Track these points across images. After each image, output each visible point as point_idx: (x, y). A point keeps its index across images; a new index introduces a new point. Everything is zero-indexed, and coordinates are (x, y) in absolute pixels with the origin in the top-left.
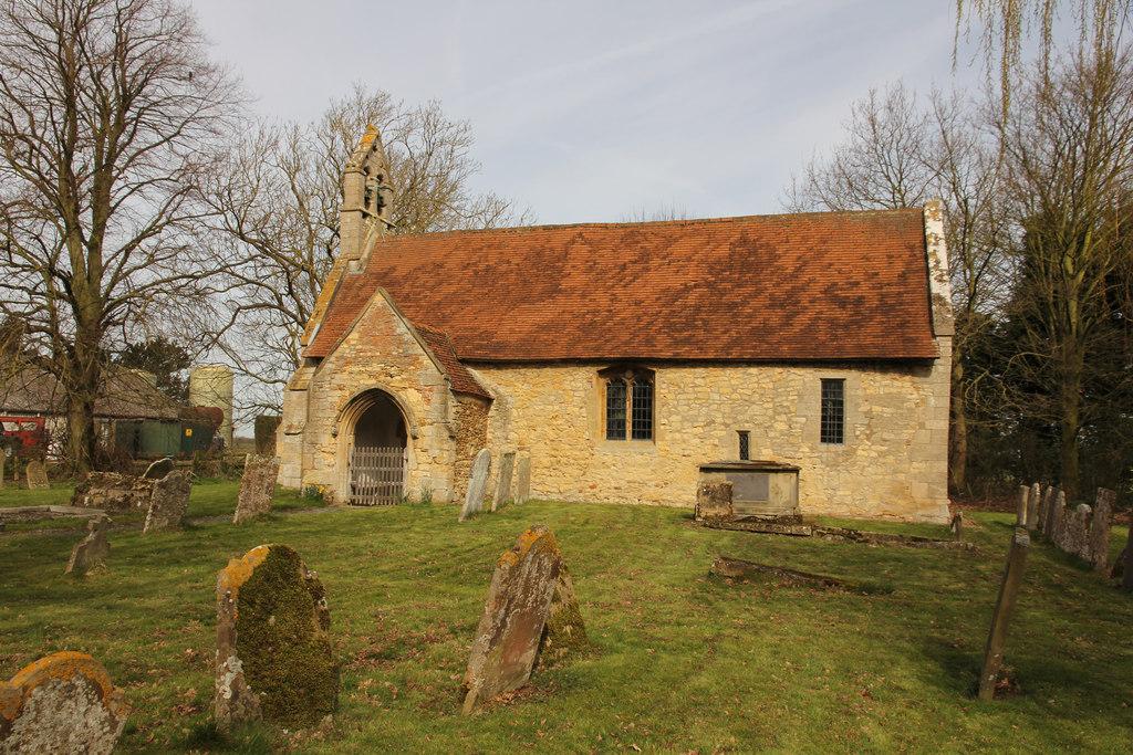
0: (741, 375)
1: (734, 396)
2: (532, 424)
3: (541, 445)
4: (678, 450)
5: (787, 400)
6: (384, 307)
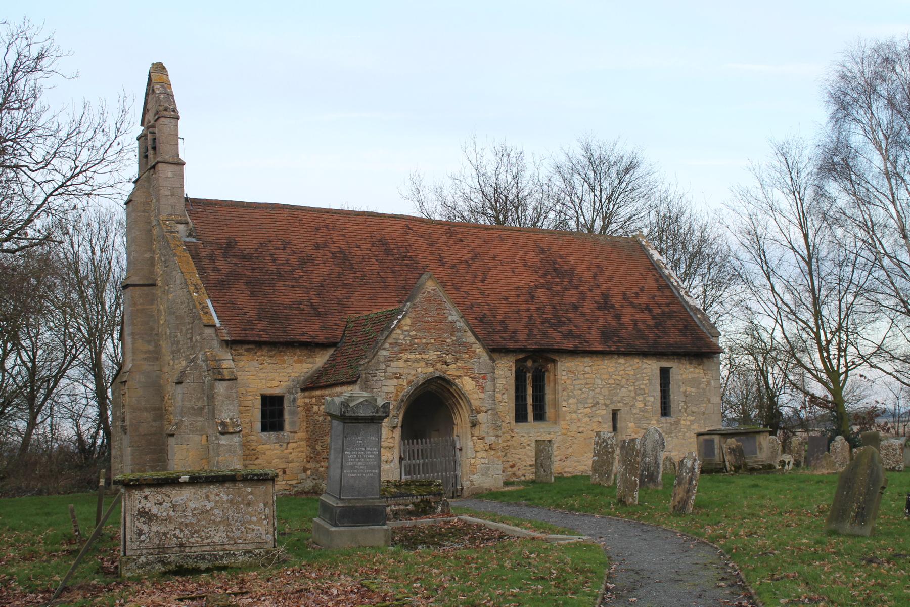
0: (614, 364)
4: (574, 428)
5: (643, 384)
6: (435, 293)
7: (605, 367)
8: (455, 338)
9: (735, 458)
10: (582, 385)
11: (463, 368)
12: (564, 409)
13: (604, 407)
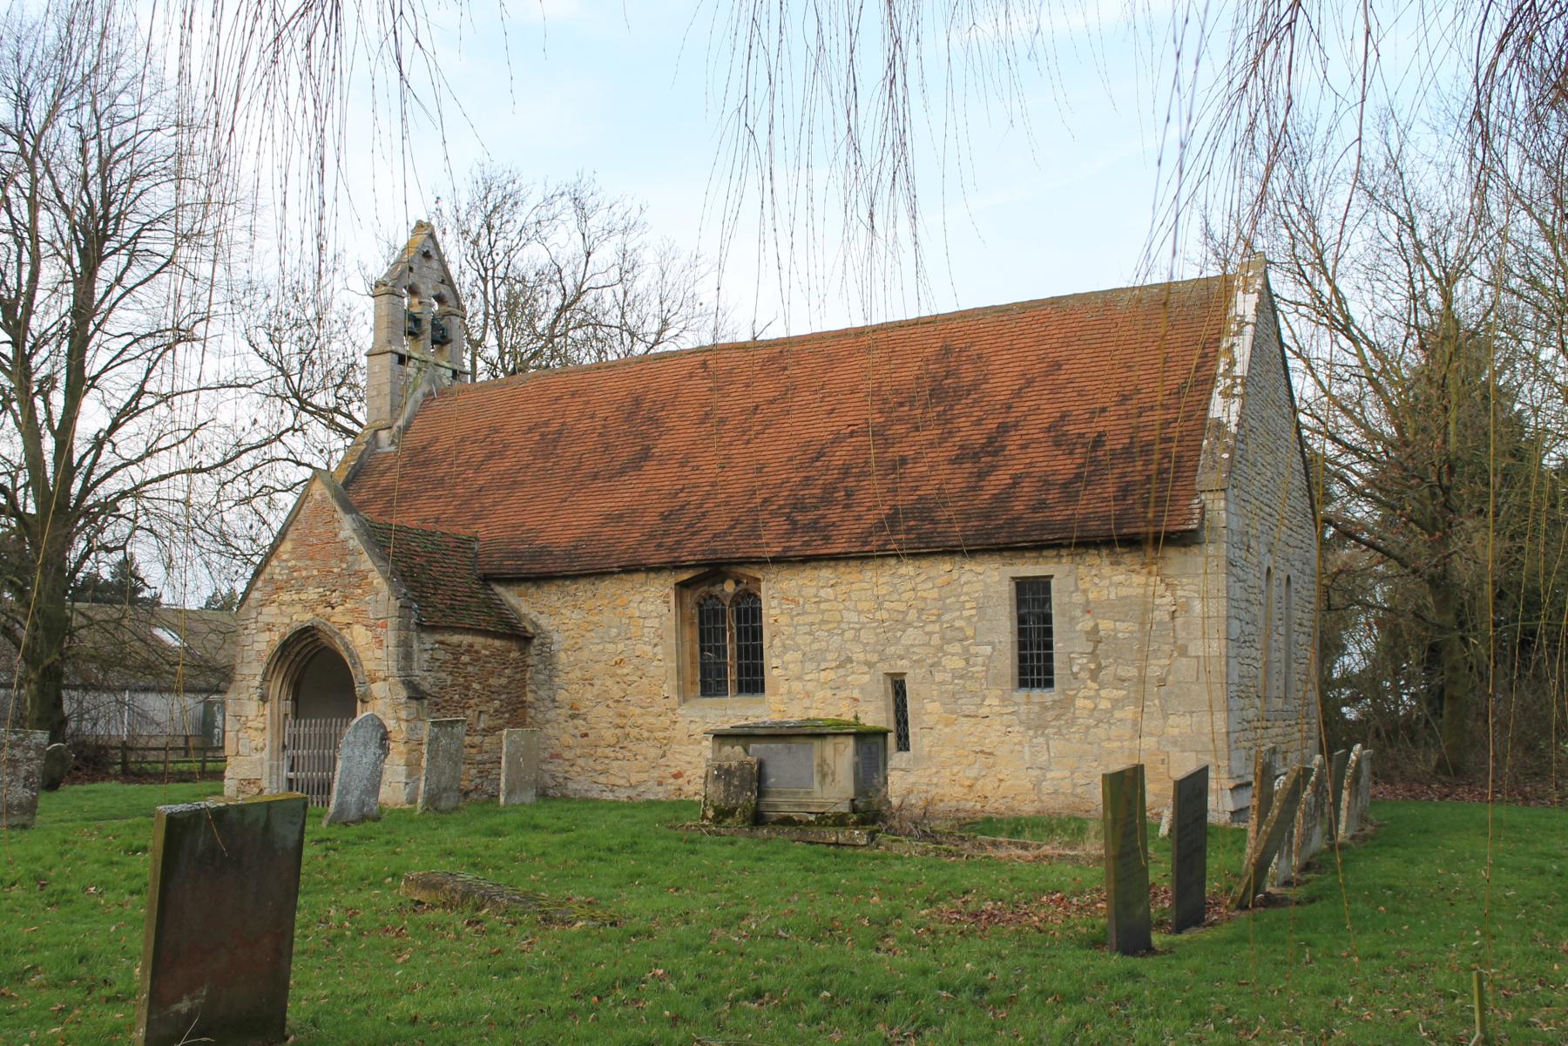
1: (878, 615)
2: (588, 675)
3: (601, 709)
5: (961, 617)
7: (865, 585)
8: (344, 566)
9: (727, 790)
10: (812, 624)
11: (352, 611)
12: (775, 672)
13: (866, 669)
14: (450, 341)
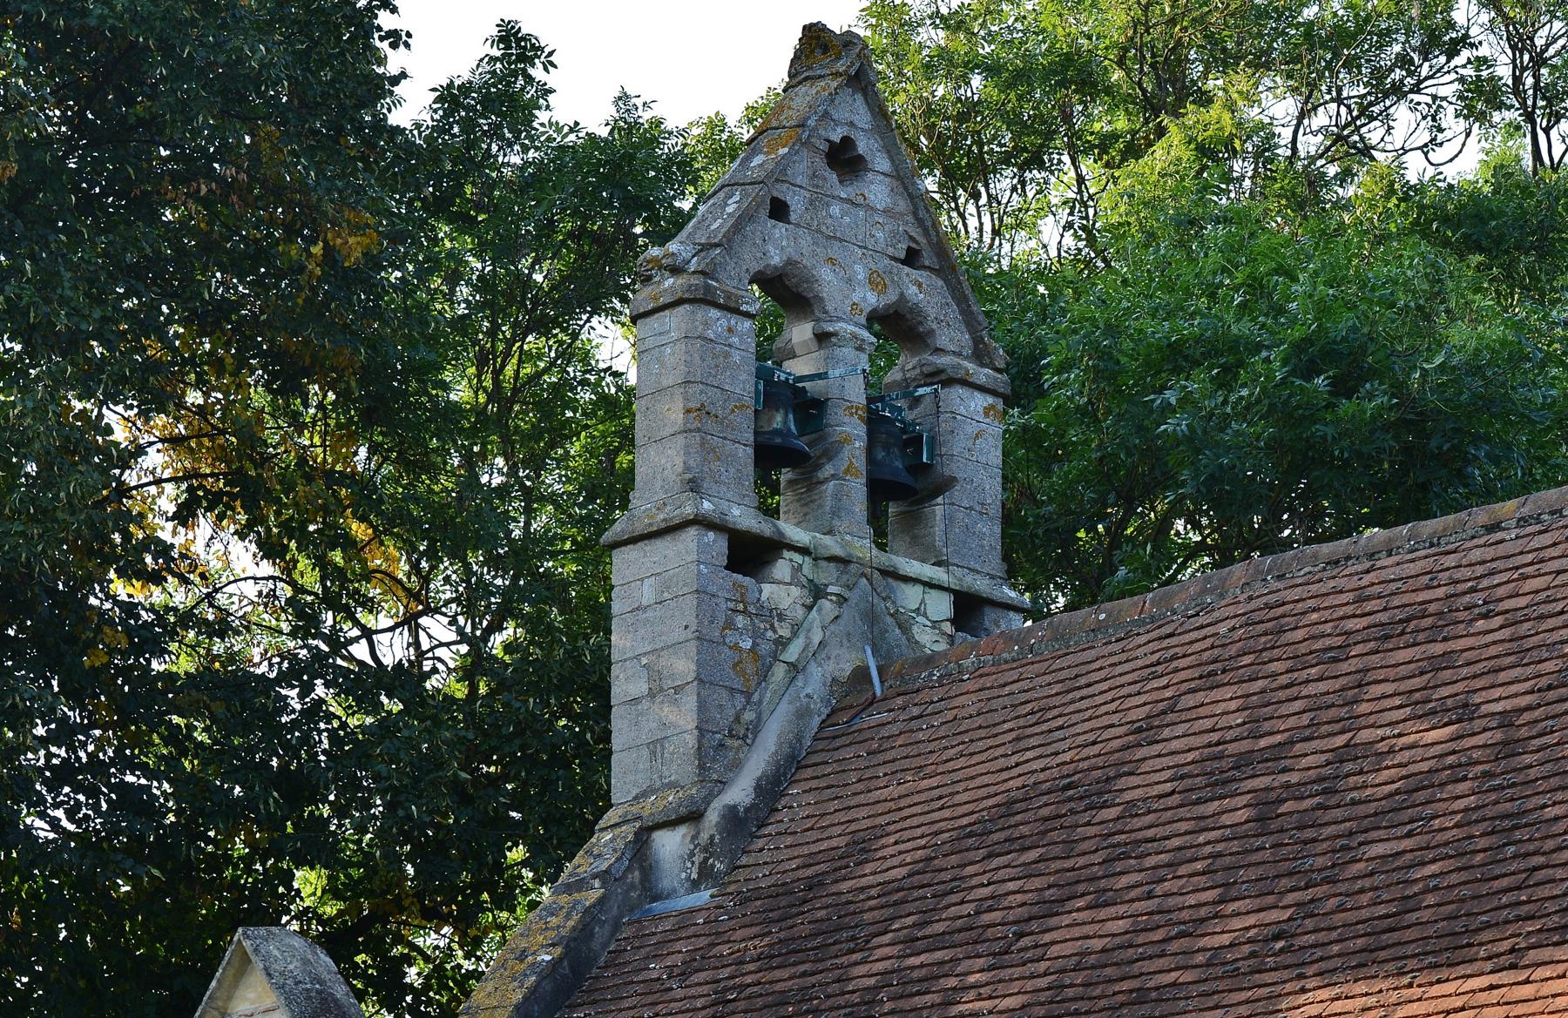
14: (945, 485)
